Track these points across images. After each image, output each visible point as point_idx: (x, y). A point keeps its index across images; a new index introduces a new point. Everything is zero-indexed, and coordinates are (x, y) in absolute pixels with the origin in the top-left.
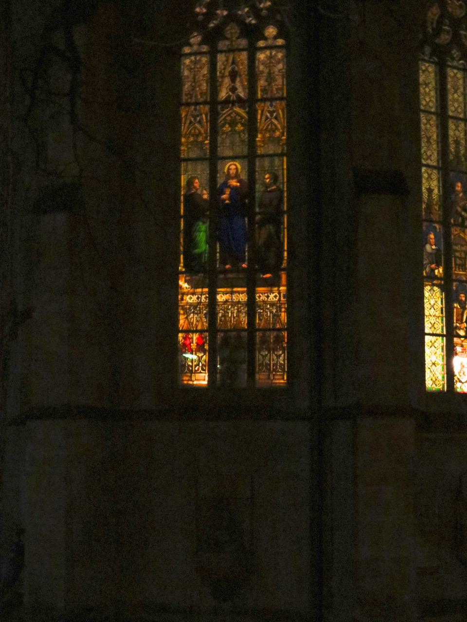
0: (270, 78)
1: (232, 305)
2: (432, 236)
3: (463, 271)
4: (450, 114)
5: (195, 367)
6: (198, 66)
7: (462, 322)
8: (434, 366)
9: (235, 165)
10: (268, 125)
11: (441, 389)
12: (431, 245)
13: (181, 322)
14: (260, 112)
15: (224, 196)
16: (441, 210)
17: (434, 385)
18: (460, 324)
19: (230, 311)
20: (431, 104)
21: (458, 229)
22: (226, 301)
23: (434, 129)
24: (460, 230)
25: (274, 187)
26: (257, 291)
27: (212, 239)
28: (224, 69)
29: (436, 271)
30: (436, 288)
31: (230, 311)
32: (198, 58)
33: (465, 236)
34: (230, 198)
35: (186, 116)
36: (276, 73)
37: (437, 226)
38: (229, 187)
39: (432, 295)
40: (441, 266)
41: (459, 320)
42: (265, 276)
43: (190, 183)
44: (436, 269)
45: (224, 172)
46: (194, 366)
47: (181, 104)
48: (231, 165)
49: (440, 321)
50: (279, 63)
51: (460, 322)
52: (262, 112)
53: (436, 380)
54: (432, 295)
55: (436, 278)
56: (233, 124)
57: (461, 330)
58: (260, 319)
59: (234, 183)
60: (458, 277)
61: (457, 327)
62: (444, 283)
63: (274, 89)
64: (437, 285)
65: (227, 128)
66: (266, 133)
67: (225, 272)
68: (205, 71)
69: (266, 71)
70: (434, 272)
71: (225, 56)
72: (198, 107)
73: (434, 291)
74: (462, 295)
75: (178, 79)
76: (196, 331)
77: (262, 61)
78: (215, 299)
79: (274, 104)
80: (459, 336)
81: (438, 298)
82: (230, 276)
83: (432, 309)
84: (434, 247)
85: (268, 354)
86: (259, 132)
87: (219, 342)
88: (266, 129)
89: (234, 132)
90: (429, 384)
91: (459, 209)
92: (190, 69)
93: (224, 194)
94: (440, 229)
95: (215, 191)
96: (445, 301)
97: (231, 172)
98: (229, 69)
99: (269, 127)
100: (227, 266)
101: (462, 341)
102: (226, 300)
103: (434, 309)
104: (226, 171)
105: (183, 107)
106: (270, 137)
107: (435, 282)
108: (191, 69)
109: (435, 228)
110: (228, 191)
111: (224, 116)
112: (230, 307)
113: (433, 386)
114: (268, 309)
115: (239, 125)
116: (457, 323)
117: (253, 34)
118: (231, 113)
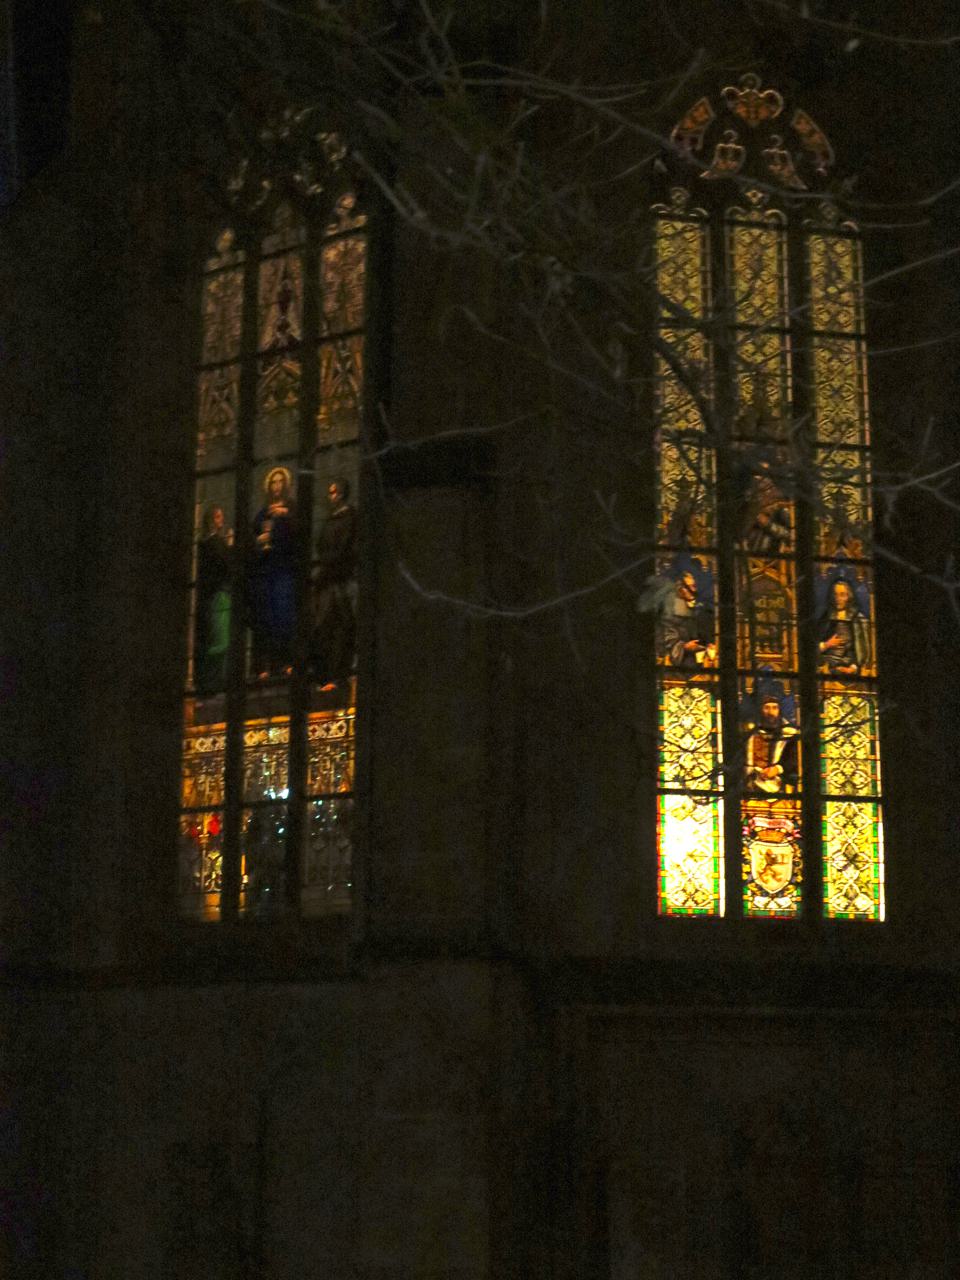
0: (344, 295)
7: (770, 764)
8: (691, 860)
10: (337, 388)
13: (187, 790)
14: (324, 363)
15: (262, 537)
16: (715, 524)
17: (690, 903)
18: (764, 768)
21: (760, 563)
24: (766, 563)
25: (344, 508)
26: (312, 719)
27: (239, 622)
28: (271, 291)
29: (700, 657)
30: (696, 692)
33: (779, 577)
34: (272, 541)
35: (207, 390)
36: (355, 282)
37: (703, 559)
38: (269, 517)
39: (687, 707)
40: (714, 644)
41: (761, 759)
42: (324, 689)
43: (207, 519)
44: (700, 650)
45: (263, 491)
46: (203, 879)
47: (199, 369)
48: (273, 475)
50: (359, 262)
52: (329, 363)
55: (700, 669)
56: (280, 394)
57: (768, 782)
59: (279, 509)
61: (754, 775)
62: (721, 678)
63: (350, 315)
64: (700, 685)
65: (271, 403)
66: (333, 403)
67: (259, 686)
68: (240, 300)
69: (338, 281)
70: (694, 658)
72: (226, 370)
73: (693, 698)
75: (196, 319)
76: (208, 809)
77: (332, 262)
78: (241, 742)
79: (348, 343)
80: (763, 795)
81: (705, 712)
82: (267, 693)
83: (688, 736)
85: (347, 846)
86: (324, 402)
87: (244, 828)
88: (334, 396)
89: (282, 408)
91: (763, 519)
92: (217, 300)
94: (709, 563)
95: (246, 526)
96: (723, 718)
98: (278, 288)
100: (264, 675)
101: (771, 805)
102: (260, 743)
103: (693, 736)
104: (266, 486)
105: (203, 373)
106: (340, 409)
107: (696, 678)
109: (698, 562)
110: (268, 525)
111: (267, 381)
113: (688, 904)
114: (327, 754)
115: (290, 395)
116: (755, 765)
117: (317, 213)
118: (279, 373)
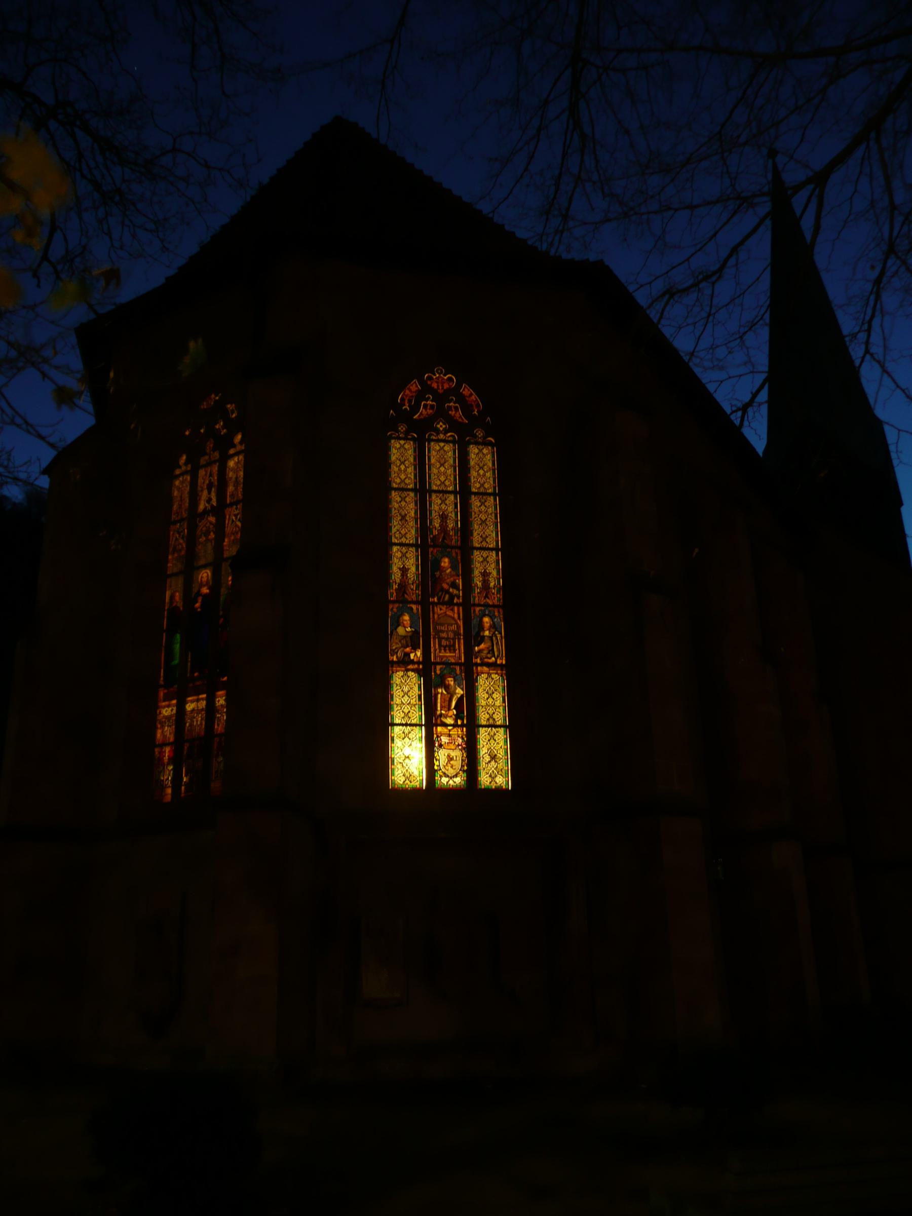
1: (197, 713)
2: (406, 617)
3: (450, 652)
4: (474, 490)
5: (166, 781)
6: (185, 485)
7: (449, 709)
9: (207, 573)
10: (233, 529)
11: (504, 787)
12: (405, 627)
18: (446, 711)
19: (195, 720)
20: (407, 481)
22: (193, 710)
23: (412, 505)
24: (446, 608)
29: (412, 656)
30: (410, 674)
31: (195, 720)
32: (185, 478)
34: (201, 607)
35: (173, 534)
38: (201, 595)
40: (420, 649)
41: (445, 707)
43: (172, 597)
44: (412, 652)
49: (417, 710)
51: (446, 709)
53: (410, 775)
54: (406, 681)
55: (412, 662)
58: (218, 725)
60: (444, 659)
61: (441, 715)
64: (413, 670)
69: (235, 476)
70: (410, 657)
71: (205, 470)
73: (409, 677)
74: (450, 679)
80: (445, 725)
82: (198, 683)
84: (409, 629)
90: (398, 778)
91: (445, 586)
93: (197, 602)
97: (203, 580)
98: (207, 482)
99: (234, 529)
101: (450, 731)
104: (199, 580)
107: (410, 667)
108: (180, 488)
110: (200, 599)
112: (195, 715)
117: (224, 445)
